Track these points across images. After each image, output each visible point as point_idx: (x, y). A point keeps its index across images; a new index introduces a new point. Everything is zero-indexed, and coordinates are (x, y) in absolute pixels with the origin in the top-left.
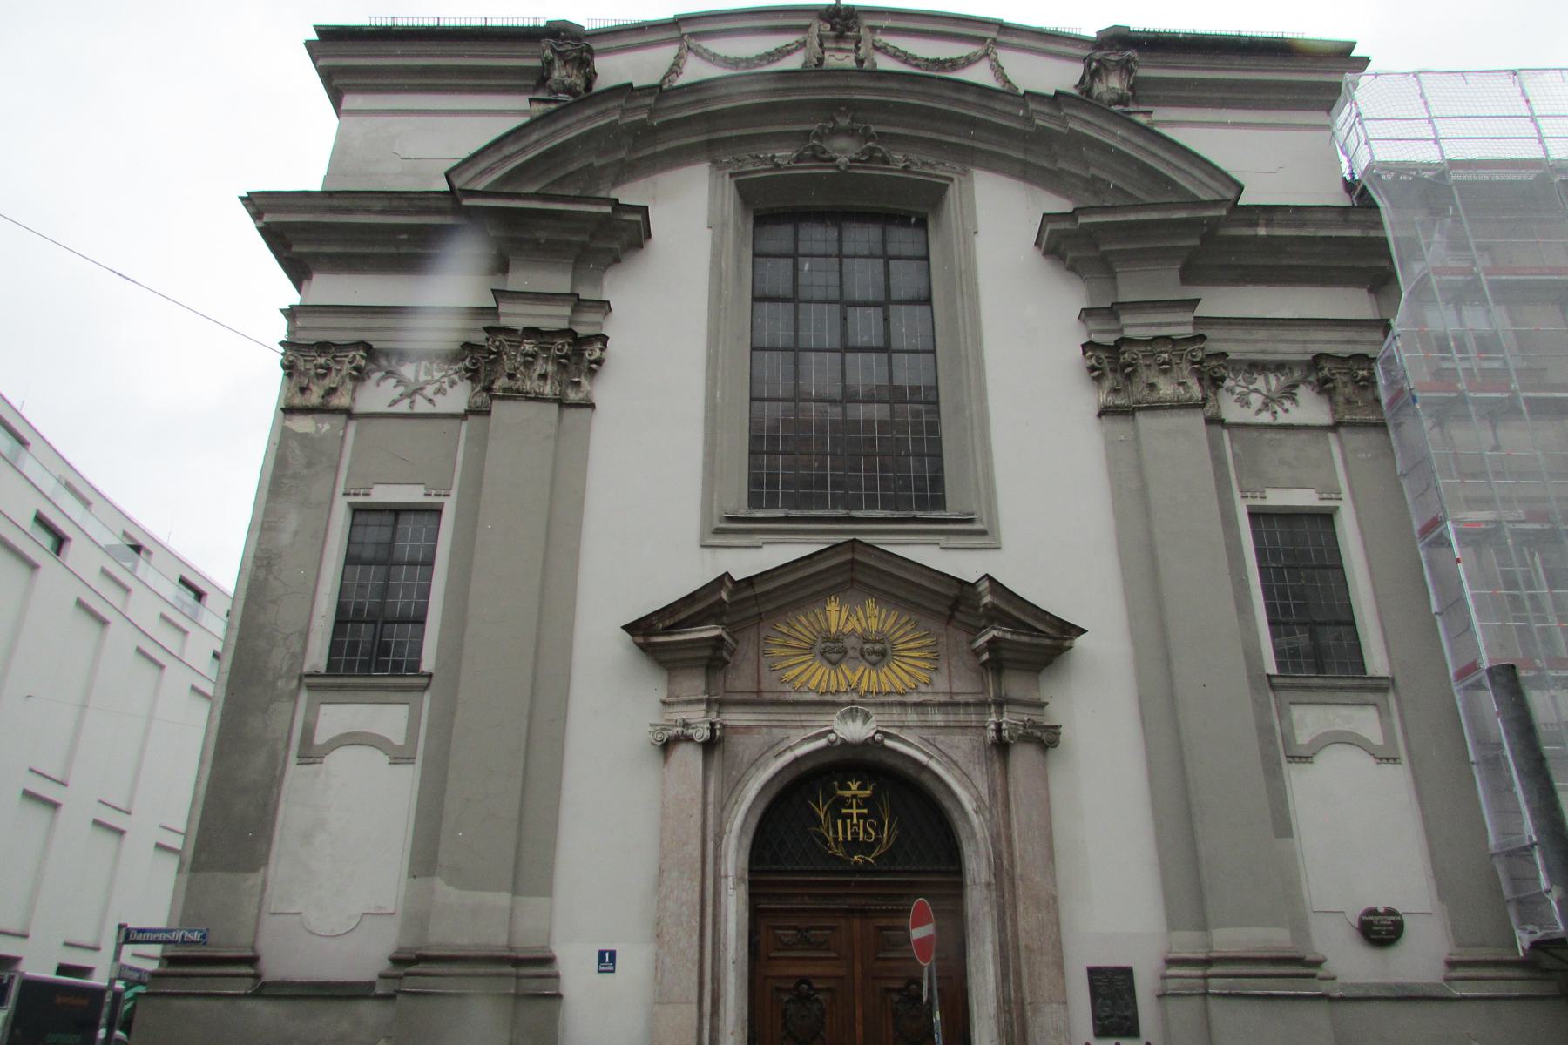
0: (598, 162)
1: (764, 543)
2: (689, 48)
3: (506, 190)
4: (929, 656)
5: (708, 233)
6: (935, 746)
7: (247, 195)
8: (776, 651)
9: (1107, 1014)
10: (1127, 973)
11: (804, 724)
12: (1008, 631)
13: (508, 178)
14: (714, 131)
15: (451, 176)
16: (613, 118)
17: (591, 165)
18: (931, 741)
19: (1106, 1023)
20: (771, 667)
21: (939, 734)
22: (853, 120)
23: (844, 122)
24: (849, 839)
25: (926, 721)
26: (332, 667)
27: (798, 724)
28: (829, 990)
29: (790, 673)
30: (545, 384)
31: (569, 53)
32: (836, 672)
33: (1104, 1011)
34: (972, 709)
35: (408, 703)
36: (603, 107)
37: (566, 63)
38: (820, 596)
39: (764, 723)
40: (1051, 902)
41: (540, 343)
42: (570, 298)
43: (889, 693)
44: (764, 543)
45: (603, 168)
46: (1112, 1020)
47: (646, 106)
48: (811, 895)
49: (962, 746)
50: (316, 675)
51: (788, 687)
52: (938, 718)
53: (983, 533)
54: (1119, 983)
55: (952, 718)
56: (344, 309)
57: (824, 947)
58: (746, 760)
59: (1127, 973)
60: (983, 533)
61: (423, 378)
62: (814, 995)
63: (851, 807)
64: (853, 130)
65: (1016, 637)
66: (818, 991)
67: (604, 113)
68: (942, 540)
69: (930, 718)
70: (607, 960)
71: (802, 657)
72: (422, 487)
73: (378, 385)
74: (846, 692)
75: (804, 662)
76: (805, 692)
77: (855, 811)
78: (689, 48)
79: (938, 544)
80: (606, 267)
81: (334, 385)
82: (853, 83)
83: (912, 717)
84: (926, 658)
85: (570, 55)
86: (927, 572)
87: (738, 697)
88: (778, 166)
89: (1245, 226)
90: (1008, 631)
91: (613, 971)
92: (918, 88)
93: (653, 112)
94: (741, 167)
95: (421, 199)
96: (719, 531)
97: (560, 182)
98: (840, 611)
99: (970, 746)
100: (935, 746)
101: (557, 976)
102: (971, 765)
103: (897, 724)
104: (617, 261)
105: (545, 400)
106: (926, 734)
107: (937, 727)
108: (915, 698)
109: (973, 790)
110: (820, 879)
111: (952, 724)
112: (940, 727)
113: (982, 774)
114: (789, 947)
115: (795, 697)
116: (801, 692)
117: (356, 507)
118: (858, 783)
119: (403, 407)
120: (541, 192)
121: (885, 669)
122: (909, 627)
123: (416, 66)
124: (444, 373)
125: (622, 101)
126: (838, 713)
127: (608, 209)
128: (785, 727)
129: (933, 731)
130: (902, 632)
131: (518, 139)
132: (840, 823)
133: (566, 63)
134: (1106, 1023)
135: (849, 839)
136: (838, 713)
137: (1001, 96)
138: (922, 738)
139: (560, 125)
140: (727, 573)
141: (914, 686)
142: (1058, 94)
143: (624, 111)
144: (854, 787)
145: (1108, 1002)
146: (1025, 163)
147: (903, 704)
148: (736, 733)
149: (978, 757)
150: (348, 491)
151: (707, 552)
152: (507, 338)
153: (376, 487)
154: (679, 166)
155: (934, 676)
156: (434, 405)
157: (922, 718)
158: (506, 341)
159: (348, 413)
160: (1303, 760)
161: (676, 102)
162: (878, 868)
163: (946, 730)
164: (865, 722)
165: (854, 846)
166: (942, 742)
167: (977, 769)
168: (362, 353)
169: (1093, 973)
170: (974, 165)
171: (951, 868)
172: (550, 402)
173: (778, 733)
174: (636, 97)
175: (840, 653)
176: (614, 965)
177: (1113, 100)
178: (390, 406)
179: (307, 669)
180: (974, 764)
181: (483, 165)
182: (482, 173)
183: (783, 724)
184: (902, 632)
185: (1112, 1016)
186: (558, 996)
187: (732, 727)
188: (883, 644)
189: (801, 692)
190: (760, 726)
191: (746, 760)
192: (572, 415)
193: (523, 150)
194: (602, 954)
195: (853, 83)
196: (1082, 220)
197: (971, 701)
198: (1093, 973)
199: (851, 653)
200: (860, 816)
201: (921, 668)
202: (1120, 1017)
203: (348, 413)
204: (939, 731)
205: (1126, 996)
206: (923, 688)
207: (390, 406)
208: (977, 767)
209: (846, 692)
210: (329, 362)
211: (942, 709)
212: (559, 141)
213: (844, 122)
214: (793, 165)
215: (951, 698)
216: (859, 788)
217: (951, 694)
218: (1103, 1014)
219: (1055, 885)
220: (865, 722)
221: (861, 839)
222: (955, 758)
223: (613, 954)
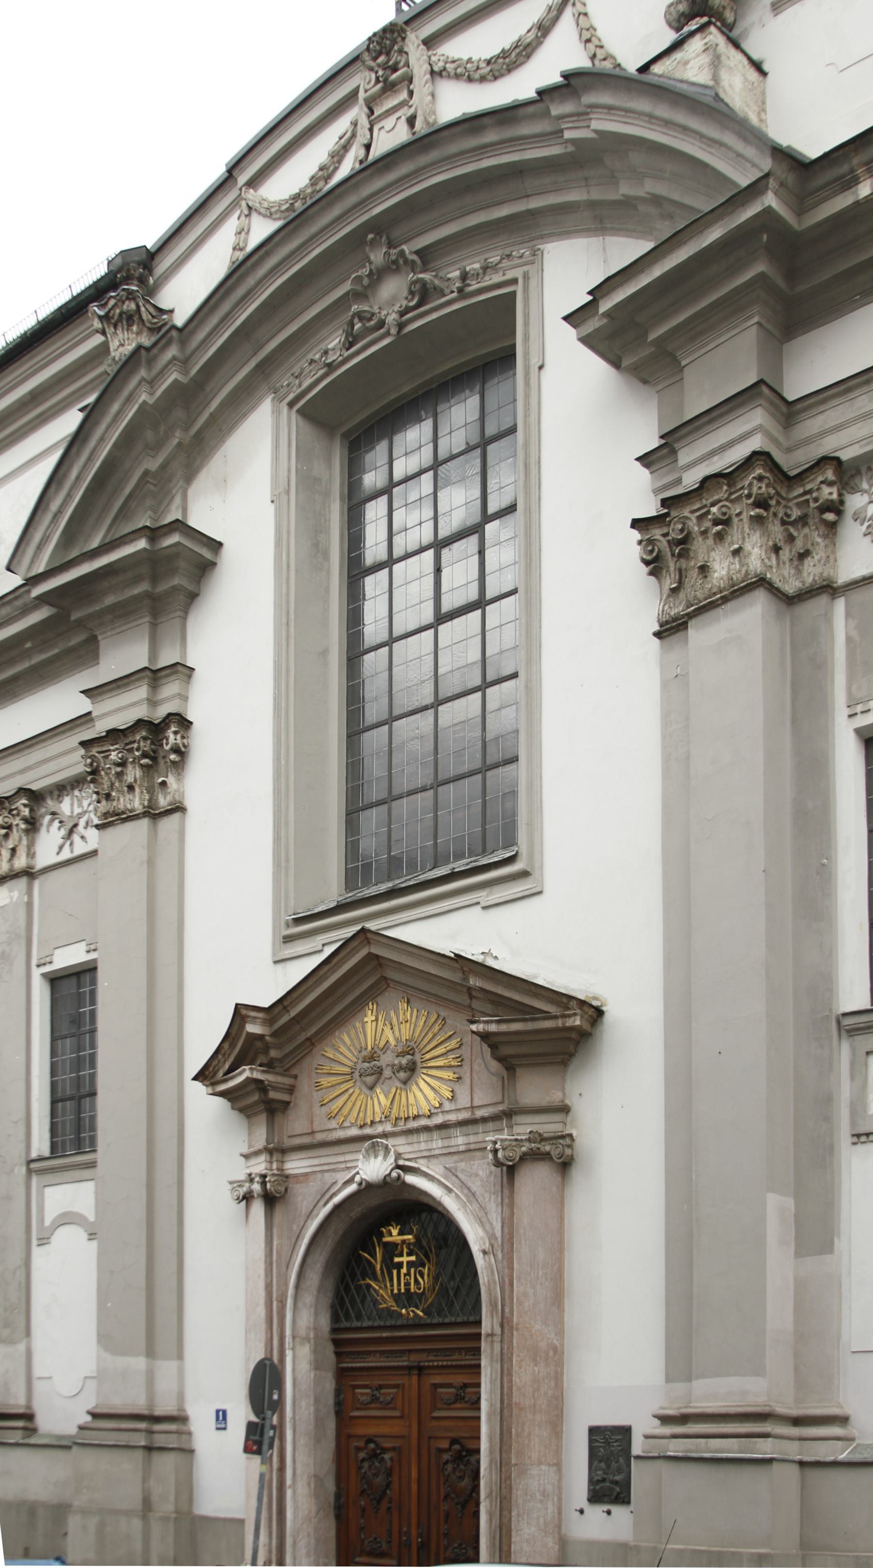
0: (153, 464)
1: (324, 945)
2: (250, 208)
3: (74, 553)
4: (452, 1063)
5: (271, 508)
6: (457, 1176)
7: (590, 298)
8: (325, 1081)
9: (600, 1478)
10: (625, 1432)
11: (349, 1165)
12: (492, 1022)
13: (69, 537)
14: (261, 347)
15: (12, 568)
16: (141, 401)
17: (146, 473)
18: (453, 1171)
19: (598, 1487)
20: (462, 1060)
21: (462, 1161)
22: (390, 245)
23: (378, 257)
24: (403, 1291)
25: (449, 1146)
26: (55, 1148)
27: (343, 1166)
28: (393, 1449)
29: (335, 1106)
30: (134, 796)
31: (112, 312)
32: (372, 1098)
33: (597, 1475)
34: (435, 1135)
35: (92, 1180)
36: (125, 393)
37: (115, 327)
38: (356, 1007)
39: (318, 1169)
40: (551, 1353)
41: (127, 744)
42: (142, 674)
43: (416, 1117)
44: (324, 945)
45: (164, 467)
46: (602, 1484)
47: (170, 362)
48: (382, 1353)
49: (480, 1172)
50: (41, 1159)
51: (334, 1124)
52: (459, 1140)
53: (524, 874)
54: (615, 1444)
55: (472, 1139)
56: (78, 722)
57: (391, 1406)
58: (303, 1212)
59: (625, 1432)
60: (524, 874)
61: (77, 810)
62: (380, 1454)
63: (401, 1255)
64: (395, 262)
65: (504, 1028)
66: (384, 1450)
67: (129, 399)
68: (483, 896)
69: (453, 1142)
70: (221, 1416)
71: (345, 1084)
72: (83, 944)
73: (48, 831)
74: (380, 1122)
75: (346, 1090)
76: (348, 1127)
77: (405, 1259)
78: (250, 208)
79: (478, 903)
80: (186, 609)
81: (736, 546)
82: (366, 191)
83: (437, 1143)
84: (450, 1067)
85: (114, 314)
86: (435, 958)
87: (298, 1141)
88: (331, 367)
89: (835, 194)
90: (492, 1022)
91: (225, 1429)
92: (434, 155)
93: (185, 362)
94: (300, 385)
95: (16, 598)
96: (288, 939)
97: (123, 513)
98: (377, 1020)
99: (488, 1171)
100: (457, 1176)
101: (190, 1434)
102: (487, 1195)
103: (425, 1154)
104: (193, 597)
105: (136, 817)
106: (450, 1162)
107: (459, 1152)
108: (438, 1120)
109: (488, 1226)
110: (385, 1335)
111: (472, 1147)
112: (462, 1152)
113: (497, 1205)
114: (365, 1406)
115: (341, 1134)
116: (345, 1127)
117: (53, 976)
118: (399, 1227)
119: (66, 855)
120: (107, 541)
121: (414, 1088)
122: (436, 1028)
123: (24, 396)
124: (90, 799)
125: (143, 373)
126: (363, 1150)
127: (142, 544)
128: (333, 1170)
129: (456, 1157)
130: (430, 1035)
131: (60, 484)
132: (395, 1272)
133: (115, 327)
134: (598, 1487)
135: (403, 1291)
136: (363, 1150)
137: (522, 112)
138: (446, 1168)
139: (92, 443)
140: (237, 1005)
141: (437, 1105)
142: (568, 76)
143: (152, 383)
144: (395, 1232)
145: (603, 1465)
146: (593, 205)
147: (427, 1129)
148: (297, 1183)
149: (494, 1186)
150: (42, 961)
151: (280, 967)
152: (100, 749)
153: (57, 952)
154: (245, 416)
155: (457, 1088)
156: (86, 842)
157: (446, 1143)
158: (99, 752)
159: (29, 874)
160: (863, 1139)
161: (201, 335)
162: (429, 1321)
163: (468, 1154)
164: (386, 1156)
165: (408, 1298)
166: (463, 1170)
167: (493, 1200)
168: (24, 801)
169: (594, 1431)
170: (543, 237)
171: (472, 1319)
172: (140, 818)
173: (329, 1178)
174: (156, 357)
175: (372, 1074)
176: (226, 1423)
177: (683, 14)
178: (58, 853)
179: (34, 1155)
180: (490, 1192)
181: (37, 536)
182: (40, 548)
183: (332, 1167)
184: (430, 1035)
185: (604, 1480)
186: (192, 1451)
187: (296, 1176)
188: (413, 1055)
189: (345, 1127)
190: (314, 1172)
191: (303, 1212)
192: (169, 824)
193: (69, 496)
194: (218, 1411)
195: (366, 191)
196: (605, 306)
197: (486, 1115)
198: (594, 1431)
199: (387, 1073)
200: (410, 1264)
201: (446, 1080)
202: (612, 1482)
203: (29, 874)
204: (462, 1156)
205: (621, 1460)
206: (447, 1106)
207: (58, 853)
208: (493, 1197)
209: (380, 1122)
210: (6, 820)
211: (464, 1128)
212: (98, 464)
213: (378, 257)
214: (346, 354)
215: (473, 1113)
216: (401, 1233)
217: (472, 1108)
218: (596, 1478)
219: (560, 1333)
220: (386, 1156)
221: (412, 1290)
222: (474, 1189)
223: (224, 1412)
